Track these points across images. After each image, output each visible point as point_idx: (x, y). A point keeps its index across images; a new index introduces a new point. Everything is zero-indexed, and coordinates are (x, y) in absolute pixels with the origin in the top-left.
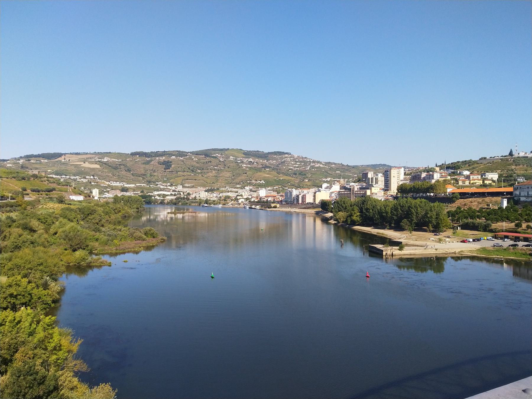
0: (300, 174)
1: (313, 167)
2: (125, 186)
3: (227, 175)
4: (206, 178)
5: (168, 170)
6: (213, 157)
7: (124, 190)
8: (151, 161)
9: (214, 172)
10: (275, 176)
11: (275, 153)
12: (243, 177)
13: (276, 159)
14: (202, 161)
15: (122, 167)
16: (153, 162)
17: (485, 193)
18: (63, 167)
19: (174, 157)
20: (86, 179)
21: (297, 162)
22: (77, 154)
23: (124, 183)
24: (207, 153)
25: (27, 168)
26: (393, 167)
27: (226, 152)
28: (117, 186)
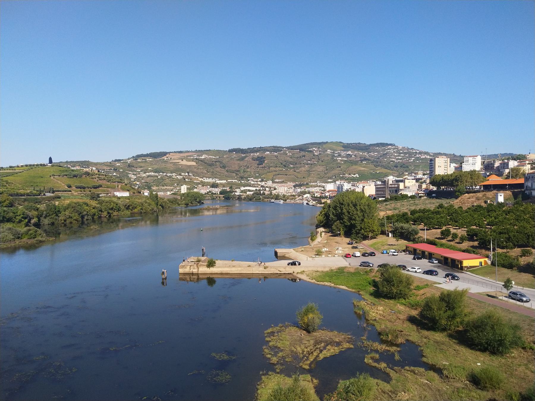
0: (401, 166)
1: (418, 159)
2: (217, 182)
3: (321, 169)
4: (298, 173)
5: (261, 166)
6: (308, 151)
7: (214, 186)
8: (246, 157)
9: (307, 166)
10: (371, 169)
11: (378, 145)
12: (337, 171)
13: (378, 151)
14: (296, 155)
15: (217, 163)
16: (247, 159)
17: (506, 185)
18: (163, 165)
19: (268, 153)
20: (181, 175)
21: (401, 153)
22: (180, 152)
23: (216, 179)
24: (302, 148)
25: (133, 166)
26: (440, 154)
27: (324, 146)
28: (209, 182)
